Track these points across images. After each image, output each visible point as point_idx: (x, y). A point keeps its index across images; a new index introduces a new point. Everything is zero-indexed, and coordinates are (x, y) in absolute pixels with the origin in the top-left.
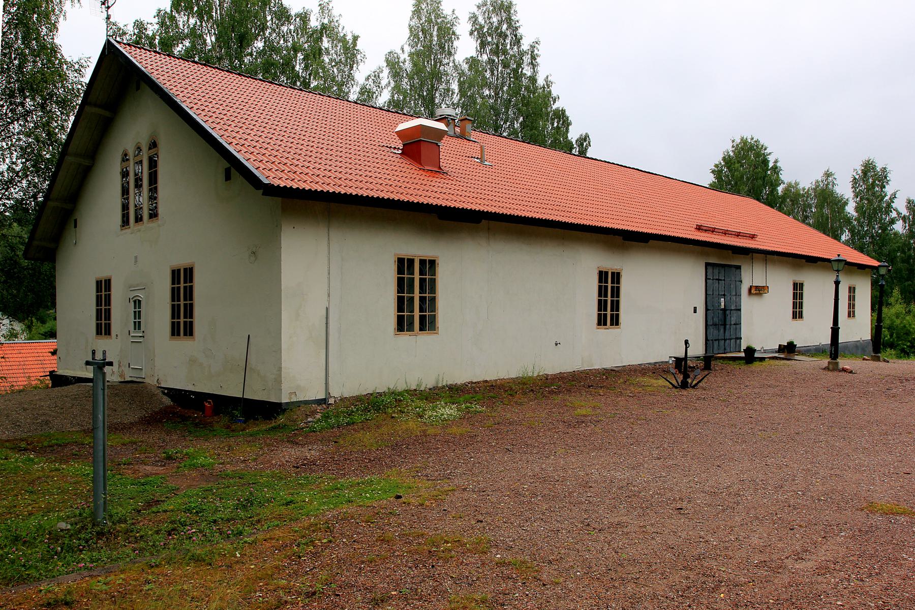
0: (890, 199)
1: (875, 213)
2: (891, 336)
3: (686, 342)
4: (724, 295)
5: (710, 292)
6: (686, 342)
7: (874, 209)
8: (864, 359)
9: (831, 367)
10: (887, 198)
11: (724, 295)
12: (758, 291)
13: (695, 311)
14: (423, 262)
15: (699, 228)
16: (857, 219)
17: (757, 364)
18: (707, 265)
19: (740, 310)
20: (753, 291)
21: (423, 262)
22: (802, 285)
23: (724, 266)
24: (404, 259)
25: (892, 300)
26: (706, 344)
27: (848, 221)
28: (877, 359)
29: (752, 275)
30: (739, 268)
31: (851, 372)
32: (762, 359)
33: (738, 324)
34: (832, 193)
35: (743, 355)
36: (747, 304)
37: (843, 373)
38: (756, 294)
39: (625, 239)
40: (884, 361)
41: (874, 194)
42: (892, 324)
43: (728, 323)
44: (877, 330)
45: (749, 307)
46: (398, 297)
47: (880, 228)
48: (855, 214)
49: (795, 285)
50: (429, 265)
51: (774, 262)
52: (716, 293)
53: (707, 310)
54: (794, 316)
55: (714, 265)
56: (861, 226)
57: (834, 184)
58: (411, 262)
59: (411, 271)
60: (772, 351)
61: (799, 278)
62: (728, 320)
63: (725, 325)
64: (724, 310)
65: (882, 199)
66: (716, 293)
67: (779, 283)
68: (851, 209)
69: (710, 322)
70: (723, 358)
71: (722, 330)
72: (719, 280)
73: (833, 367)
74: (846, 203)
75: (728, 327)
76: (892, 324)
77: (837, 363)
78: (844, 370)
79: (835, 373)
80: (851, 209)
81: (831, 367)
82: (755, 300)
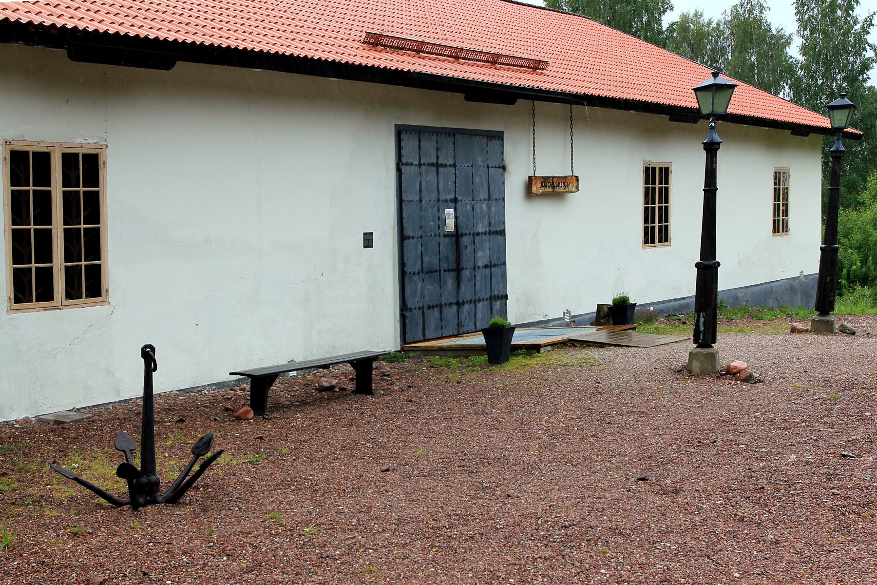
0: (863, 28)
1: (837, 53)
2: (864, 261)
3: (148, 355)
4: (455, 201)
5: (411, 195)
6: (148, 355)
7: (836, 47)
8: (794, 330)
9: (696, 366)
10: (857, 27)
11: (455, 201)
12: (550, 189)
13: (368, 241)
14: (69, 160)
15: (374, 41)
16: (806, 67)
17: (515, 363)
18: (400, 132)
19: (502, 233)
20: (536, 188)
21: (69, 160)
22: (665, 172)
23: (452, 133)
24: (76, 155)
25: (865, 196)
26: (403, 317)
27: (789, 69)
28: (824, 327)
29: (527, 155)
30: (498, 136)
31: (749, 379)
32: (534, 349)
33: (498, 264)
34: (758, 22)
35: (479, 340)
36: (520, 218)
37: (727, 385)
38: (543, 195)
39: (73, 56)
40: (844, 331)
41: (833, 22)
42: (866, 239)
43: (467, 262)
44: (829, 256)
45: (525, 227)
46: (98, 221)
47: (845, 79)
48: (801, 58)
49: (650, 173)
50: (85, 168)
51: (593, 125)
52: (429, 197)
53: (402, 237)
54: (649, 238)
55: (419, 131)
56: (812, 77)
57: (762, 9)
58: (43, 159)
59: (44, 177)
60: (576, 321)
61: (658, 157)
62: (467, 254)
63: (458, 270)
64: (456, 236)
65: (848, 32)
66: (429, 197)
67: (611, 176)
68: (794, 52)
69: (413, 266)
70: (441, 349)
71: (450, 282)
72: (437, 166)
73: (704, 366)
74: (788, 43)
75: (466, 274)
76: (866, 239)
77: (713, 357)
78: (731, 373)
79: (706, 385)
80: (794, 52)
81: (696, 366)
82: (546, 212)
